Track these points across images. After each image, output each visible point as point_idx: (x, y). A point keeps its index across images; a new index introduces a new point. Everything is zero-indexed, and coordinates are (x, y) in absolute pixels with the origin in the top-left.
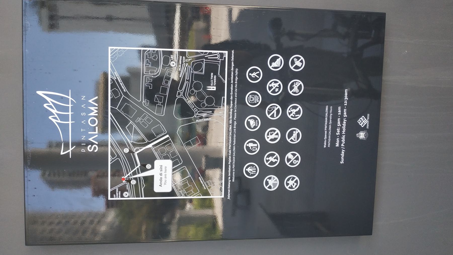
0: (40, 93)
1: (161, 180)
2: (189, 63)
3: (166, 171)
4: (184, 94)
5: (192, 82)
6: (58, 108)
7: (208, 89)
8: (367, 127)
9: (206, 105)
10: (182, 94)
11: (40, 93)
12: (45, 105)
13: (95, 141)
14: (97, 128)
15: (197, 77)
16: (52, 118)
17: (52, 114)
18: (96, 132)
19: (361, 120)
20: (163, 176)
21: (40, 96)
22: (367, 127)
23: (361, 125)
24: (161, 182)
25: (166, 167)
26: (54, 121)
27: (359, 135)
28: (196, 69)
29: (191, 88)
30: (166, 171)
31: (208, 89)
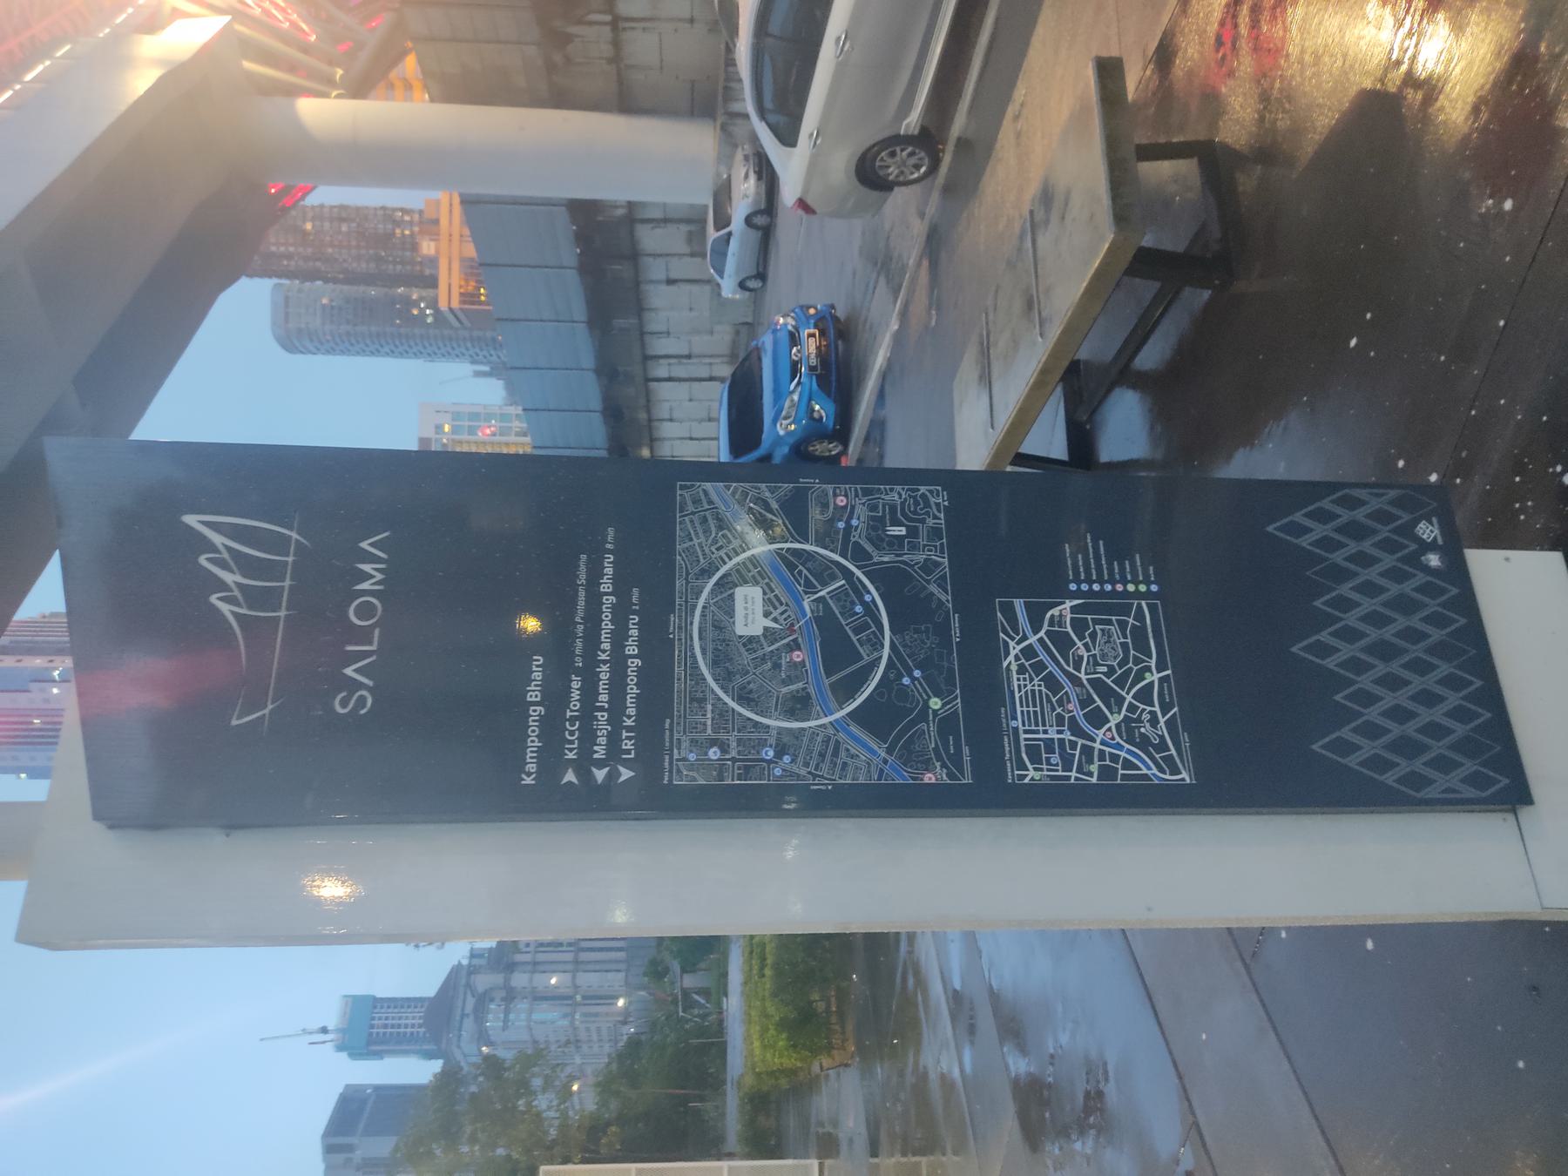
0: (191, 520)
1: (746, 616)
2: (864, 504)
3: (753, 602)
4: (860, 537)
5: (868, 524)
6: (245, 565)
7: (888, 533)
8: (1440, 541)
9: (887, 548)
10: (857, 536)
11: (191, 520)
12: (203, 560)
13: (367, 676)
14: (377, 632)
15: (873, 518)
16: (219, 599)
17: (222, 586)
18: (372, 645)
19: (1421, 528)
20: (750, 612)
21: (192, 528)
22: (1440, 541)
23: (1425, 537)
24: (746, 620)
25: (753, 598)
26: (225, 608)
27: (1427, 560)
28: (871, 511)
29: (867, 530)
30: (753, 602)
31: (888, 533)
